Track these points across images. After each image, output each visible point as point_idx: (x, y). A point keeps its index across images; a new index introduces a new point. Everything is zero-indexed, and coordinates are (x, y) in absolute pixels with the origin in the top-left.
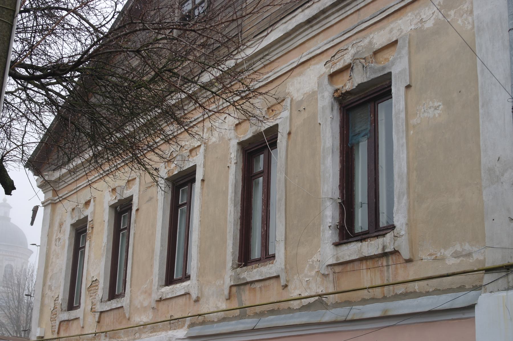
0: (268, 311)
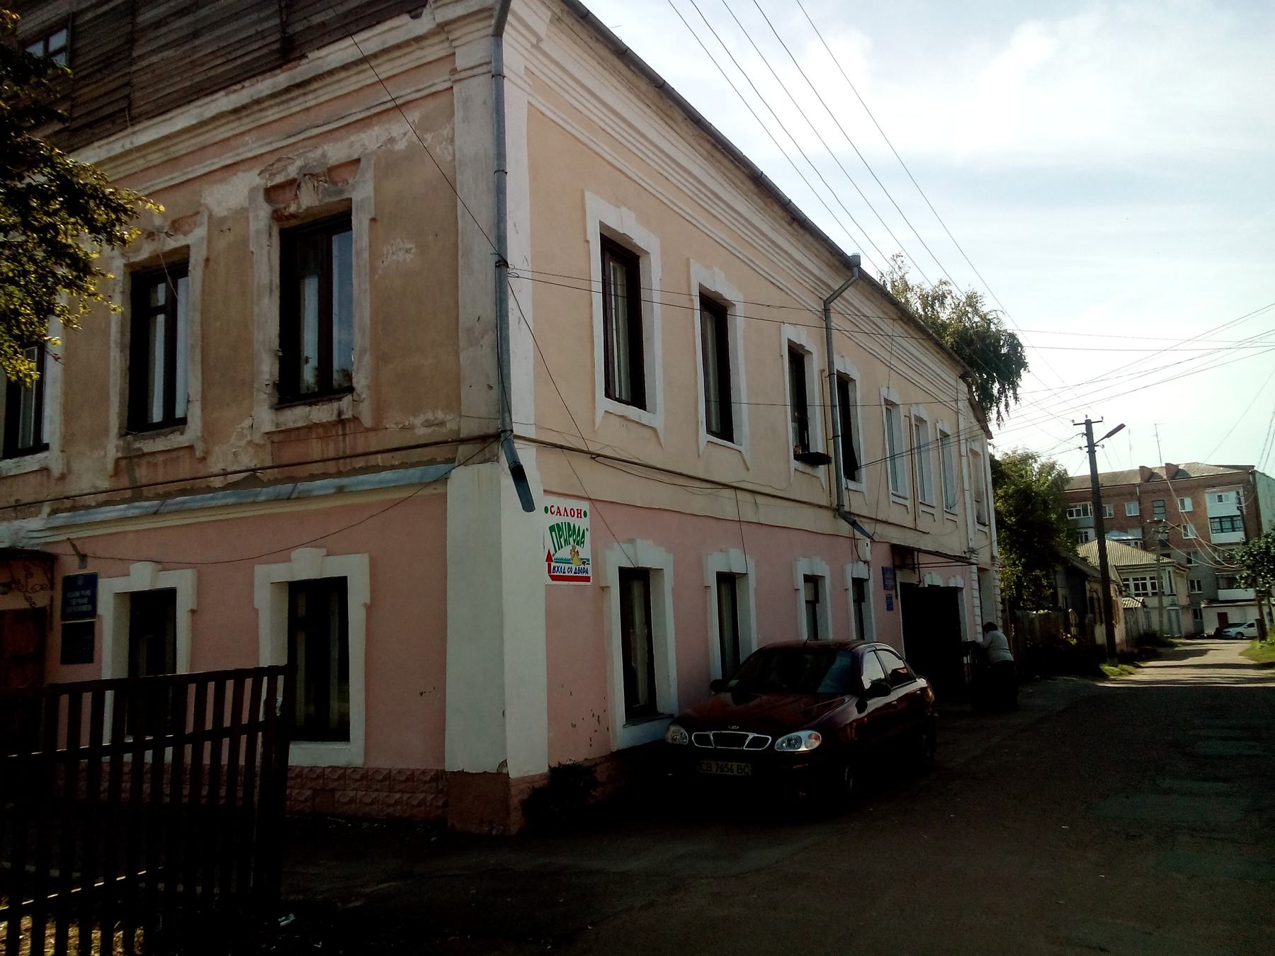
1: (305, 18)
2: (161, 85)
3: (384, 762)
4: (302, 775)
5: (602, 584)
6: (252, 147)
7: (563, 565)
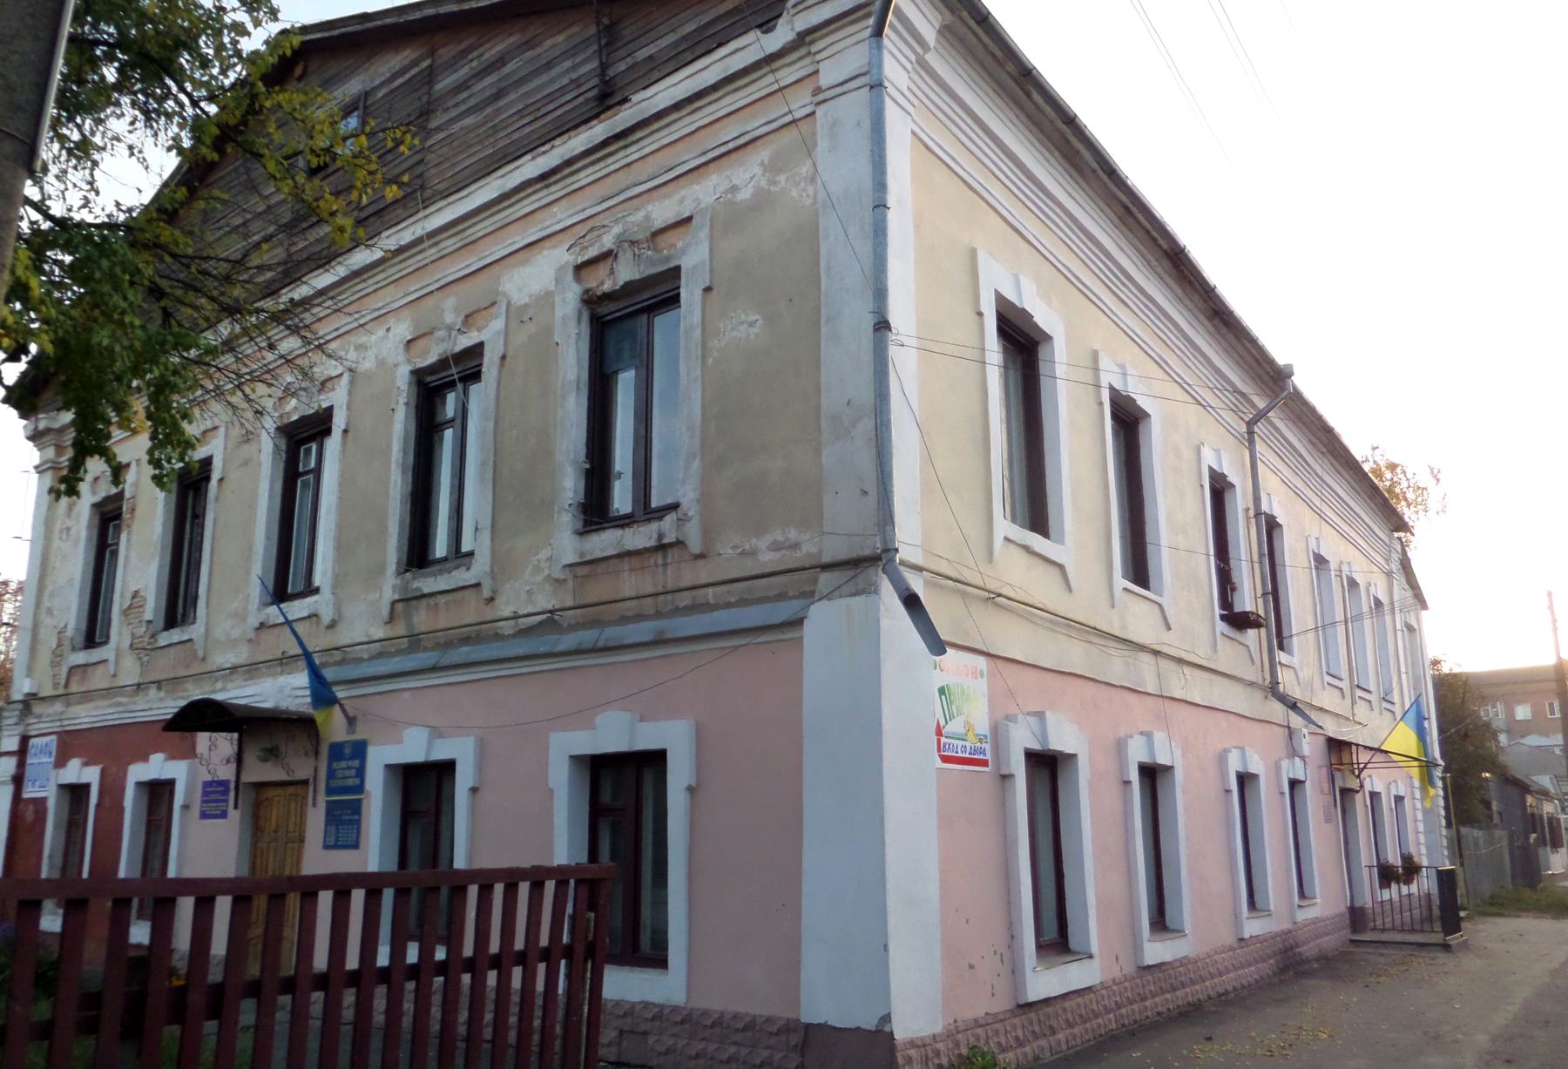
0: (458, 640)
1: (629, 55)
2: (460, 158)
3: (716, 1002)
5: (1004, 772)
6: (561, 216)
7: (955, 742)
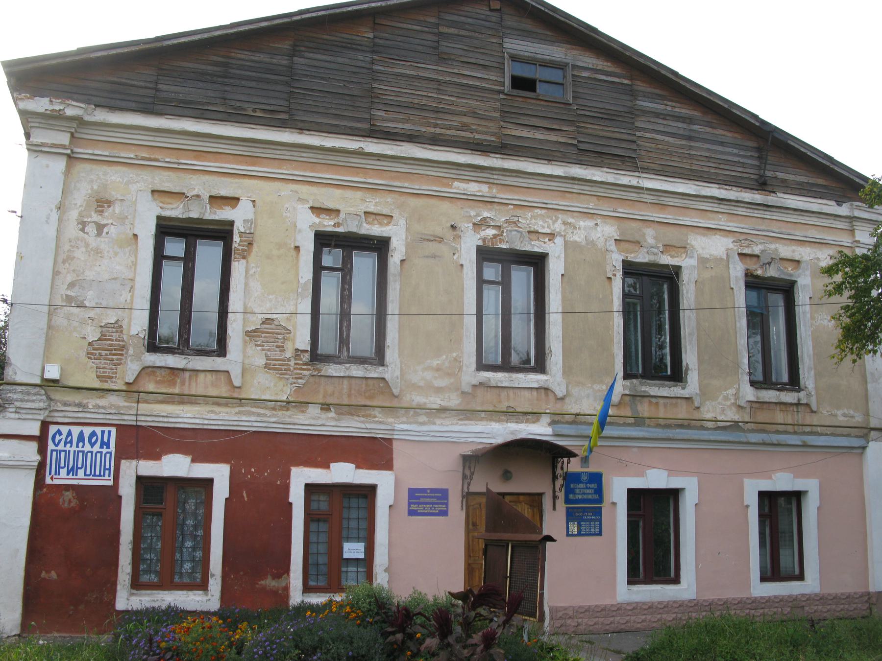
0: (675, 425)
4: (605, 610)
